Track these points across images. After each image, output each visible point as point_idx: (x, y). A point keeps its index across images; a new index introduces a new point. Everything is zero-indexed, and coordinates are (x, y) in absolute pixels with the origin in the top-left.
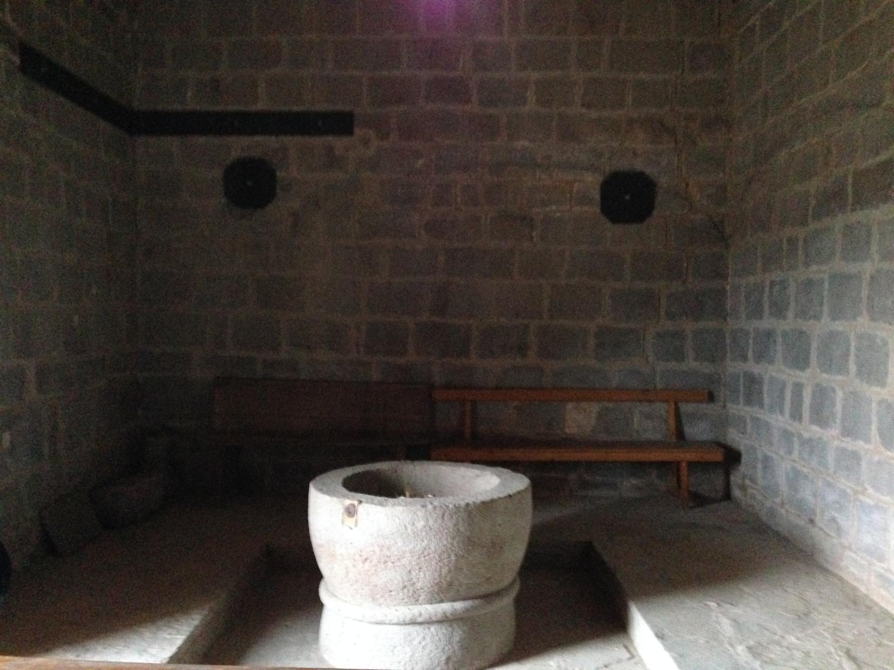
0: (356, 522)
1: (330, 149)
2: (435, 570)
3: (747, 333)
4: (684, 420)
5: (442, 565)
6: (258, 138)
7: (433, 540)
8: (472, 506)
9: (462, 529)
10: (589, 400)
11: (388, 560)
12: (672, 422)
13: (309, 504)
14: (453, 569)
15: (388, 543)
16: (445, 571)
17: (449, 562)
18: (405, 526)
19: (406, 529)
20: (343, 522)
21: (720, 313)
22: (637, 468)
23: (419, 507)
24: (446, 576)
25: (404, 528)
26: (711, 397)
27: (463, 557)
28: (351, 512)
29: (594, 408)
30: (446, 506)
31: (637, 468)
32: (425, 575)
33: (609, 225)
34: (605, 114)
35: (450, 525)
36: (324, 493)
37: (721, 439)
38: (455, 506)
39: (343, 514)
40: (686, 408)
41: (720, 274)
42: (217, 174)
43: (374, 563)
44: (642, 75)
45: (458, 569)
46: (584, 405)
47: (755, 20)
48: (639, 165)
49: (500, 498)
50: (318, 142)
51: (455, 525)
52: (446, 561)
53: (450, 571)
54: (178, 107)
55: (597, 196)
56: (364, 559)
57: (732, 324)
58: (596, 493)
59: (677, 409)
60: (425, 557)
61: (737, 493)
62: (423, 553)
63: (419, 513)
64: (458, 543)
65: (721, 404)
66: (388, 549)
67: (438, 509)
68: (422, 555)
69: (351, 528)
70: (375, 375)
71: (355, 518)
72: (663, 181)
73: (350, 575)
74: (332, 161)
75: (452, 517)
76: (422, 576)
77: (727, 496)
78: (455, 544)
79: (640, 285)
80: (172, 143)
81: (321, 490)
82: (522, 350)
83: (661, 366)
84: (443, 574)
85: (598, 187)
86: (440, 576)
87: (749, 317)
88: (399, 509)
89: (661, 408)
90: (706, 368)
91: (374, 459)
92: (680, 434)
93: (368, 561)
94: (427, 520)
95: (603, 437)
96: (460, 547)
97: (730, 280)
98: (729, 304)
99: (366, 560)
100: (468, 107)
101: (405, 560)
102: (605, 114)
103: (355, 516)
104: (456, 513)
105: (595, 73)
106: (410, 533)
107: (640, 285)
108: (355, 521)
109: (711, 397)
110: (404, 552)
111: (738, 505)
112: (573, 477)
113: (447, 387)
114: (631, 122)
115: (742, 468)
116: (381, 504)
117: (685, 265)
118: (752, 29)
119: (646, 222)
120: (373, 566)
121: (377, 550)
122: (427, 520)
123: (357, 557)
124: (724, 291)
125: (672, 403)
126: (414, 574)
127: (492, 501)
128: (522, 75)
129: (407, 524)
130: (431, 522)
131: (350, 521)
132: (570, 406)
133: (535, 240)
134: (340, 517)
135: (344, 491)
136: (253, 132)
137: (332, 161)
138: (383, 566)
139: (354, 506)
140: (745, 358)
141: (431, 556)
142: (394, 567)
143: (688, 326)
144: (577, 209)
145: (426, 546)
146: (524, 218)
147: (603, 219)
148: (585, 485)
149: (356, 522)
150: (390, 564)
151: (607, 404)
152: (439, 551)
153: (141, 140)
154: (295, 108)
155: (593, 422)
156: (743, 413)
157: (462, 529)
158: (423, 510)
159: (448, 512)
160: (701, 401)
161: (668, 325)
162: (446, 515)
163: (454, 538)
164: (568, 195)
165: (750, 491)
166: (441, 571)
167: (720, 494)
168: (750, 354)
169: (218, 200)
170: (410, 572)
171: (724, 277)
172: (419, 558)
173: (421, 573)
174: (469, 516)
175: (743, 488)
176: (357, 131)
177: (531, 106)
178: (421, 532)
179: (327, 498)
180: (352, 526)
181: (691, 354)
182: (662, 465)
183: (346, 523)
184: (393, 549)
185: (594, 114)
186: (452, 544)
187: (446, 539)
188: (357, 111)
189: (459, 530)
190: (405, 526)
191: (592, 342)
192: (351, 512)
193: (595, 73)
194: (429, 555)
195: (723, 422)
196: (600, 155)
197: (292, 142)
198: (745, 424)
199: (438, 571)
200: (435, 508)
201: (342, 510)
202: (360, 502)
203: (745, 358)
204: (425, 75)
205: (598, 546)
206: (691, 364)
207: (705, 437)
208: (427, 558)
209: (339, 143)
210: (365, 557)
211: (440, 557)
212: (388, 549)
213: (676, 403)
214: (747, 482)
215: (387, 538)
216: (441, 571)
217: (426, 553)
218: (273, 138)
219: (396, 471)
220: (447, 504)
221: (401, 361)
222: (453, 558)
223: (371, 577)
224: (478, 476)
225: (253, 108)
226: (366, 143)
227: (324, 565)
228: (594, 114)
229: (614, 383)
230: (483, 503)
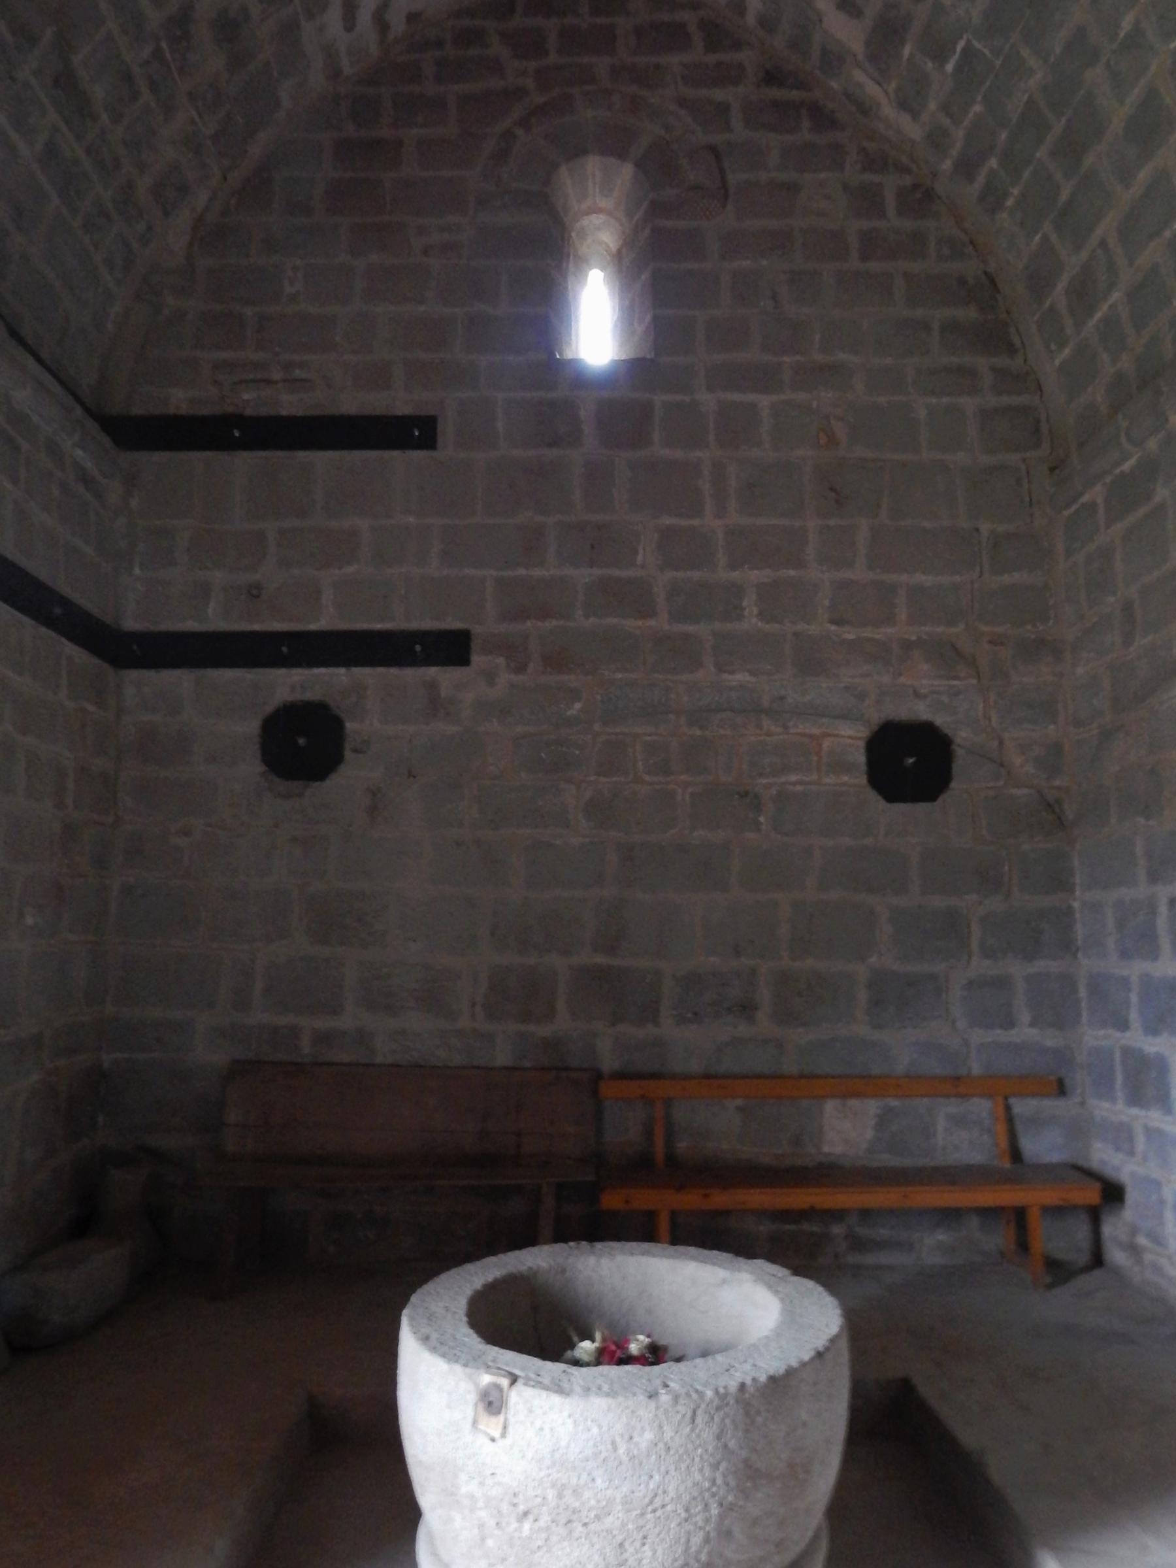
0: (505, 1427)
1: (432, 686)
2: (677, 1541)
3: (1125, 982)
4: (1019, 1127)
5: (692, 1527)
6: (317, 671)
7: (672, 1472)
8: (752, 1390)
9: (732, 1444)
10: (858, 1095)
11: (574, 1517)
12: (1001, 1128)
13: (398, 1372)
14: (713, 1534)
15: (574, 1481)
16: (697, 1540)
17: (707, 1520)
18: (613, 1443)
19: (615, 1449)
20: (475, 1423)
21: (1067, 946)
22: (950, 1216)
23: (641, 1398)
24: (699, 1552)
25: (610, 1447)
26: (1061, 1089)
27: (732, 1507)
28: (492, 1403)
29: (872, 1107)
30: (697, 1391)
31: (950, 1216)
32: (655, 1552)
33: (882, 804)
34: (868, 632)
35: (708, 1435)
36: (433, 1350)
37: (1081, 1162)
38: (717, 1392)
39: (476, 1405)
40: (1022, 1107)
41: (1060, 881)
42: (251, 727)
43: (542, 1523)
44: (920, 578)
45: (726, 1534)
46: (853, 1103)
47: (1096, 494)
48: (922, 711)
49: (804, 1365)
50: (411, 675)
51: (719, 1437)
52: (699, 1519)
53: (707, 1540)
54: (192, 626)
55: (861, 758)
56: (521, 1513)
57: (1087, 965)
58: (884, 1258)
59: (1008, 1108)
60: (654, 1511)
61: (1116, 1256)
62: (651, 1502)
63: (641, 1412)
64: (724, 1476)
65: (1078, 1099)
66: (576, 1492)
67: (682, 1401)
68: (650, 1508)
69: (493, 1440)
70: (502, 1056)
71: (501, 1418)
72: (962, 736)
73: (490, 1543)
74: (435, 705)
75: (713, 1418)
76: (649, 1554)
77: (1097, 1259)
78: (719, 1481)
79: (939, 902)
80: (181, 680)
81: (425, 1340)
82: (747, 1009)
83: (978, 1036)
84: (693, 1549)
85: (862, 744)
86: (686, 1550)
87: (1125, 954)
88: (599, 1403)
89: (981, 1107)
90: (1051, 1039)
91: (525, 1239)
92: (1016, 1155)
93: (531, 1517)
94: (660, 1427)
95: (887, 1160)
96: (727, 1485)
97: (1078, 893)
98: (1080, 932)
99: (526, 1514)
100: (652, 622)
101: (610, 1519)
102: (868, 632)
103: (503, 1410)
104: (718, 1409)
105: (846, 574)
106: (625, 1458)
107: (939, 902)
108: (500, 1426)
109: (1061, 1089)
110: (611, 1501)
111: (1117, 1272)
112: (837, 1230)
113: (621, 1076)
114: (907, 646)
115: (1128, 1213)
116: (558, 1389)
117: (1006, 868)
118: (1092, 507)
119: (940, 800)
120: (540, 1530)
121: (551, 1494)
122: (660, 1427)
123: (505, 1508)
124: (1070, 911)
125: (1000, 1099)
126: (631, 1550)
127: (790, 1373)
128: (735, 575)
129: (618, 1439)
130: (669, 1433)
131: (492, 1425)
132: (830, 1106)
133: (764, 827)
134: (470, 1412)
135: (473, 1340)
136: (312, 663)
137: (435, 705)
138: (562, 1531)
139: (498, 1387)
140: (1124, 1026)
141: (669, 1508)
142: (588, 1534)
143: (1017, 969)
144: (830, 780)
145: (658, 1487)
146: (746, 793)
147: (872, 796)
148: (859, 1244)
149: (505, 1427)
150: (579, 1529)
151: (894, 1103)
152: (686, 1498)
153: (133, 674)
154: (379, 626)
155: (869, 1134)
156: (1124, 1118)
157: (732, 1444)
158: (652, 1405)
159: (703, 1406)
160: (1048, 1096)
161: (979, 967)
162: (699, 1412)
163: (715, 1466)
164: (815, 758)
165: (1148, 1257)
166: (688, 1541)
167: (1084, 1259)
168: (1134, 1016)
169: (251, 767)
170: (621, 1545)
171: (1070, 889)
172: (643, 1514)
173: (646, 1548)
174: (747, 1414)
175: (1134, 1250)
176: (475, 658)
177: (751, 621)
178: (648, 1456)
179: (440, 1365)
180: (496, 1434)
181: (1025, 1017)
182: (988, 1213)
183: (482, 1427)
184: (587, 1494)
185: (850, 634)
186: (714, 1482)
187: (701, 1470)
188: (476, 629)
189: (725, 1446)
190: (613, 1443)
191: (862, 996)
192: (492, 1403)
193: (846, 574)
194: (663, 1506)
195: (1078, 1130)
196: (862, 697)
197: (367, 675)
198: (1131, 1139)
199: (683, 1540)
200: (676, 1398)
201: (472, 1397)
202: (514, 1380)
203: (1124, 1026)
204: (583, 575)
205: (925, 1390)
206: (1025, 1032)
207: (1055, 1157)
208: (658, 1513)
209: (445, 677)
210: (522, 1508)
211: (687, 1510)
212: (576, 1492)
213: (1006, 1098)
214: (1142, 1240)
215: (574, 1468)
216: (688, 1541)
217: (658, 1502)
218: (342, 670)
219: (564, 1271)
220: (699, 1387)
221: (544, 1031)
222: (715, 1511)
223: (535, 1553)
224: (724, 1281)
225: (313, 627)
226: (490, 677)
227: (427, 1497)
228: (850, 634)
229: (900, 1068)
230: (772, 1379)
